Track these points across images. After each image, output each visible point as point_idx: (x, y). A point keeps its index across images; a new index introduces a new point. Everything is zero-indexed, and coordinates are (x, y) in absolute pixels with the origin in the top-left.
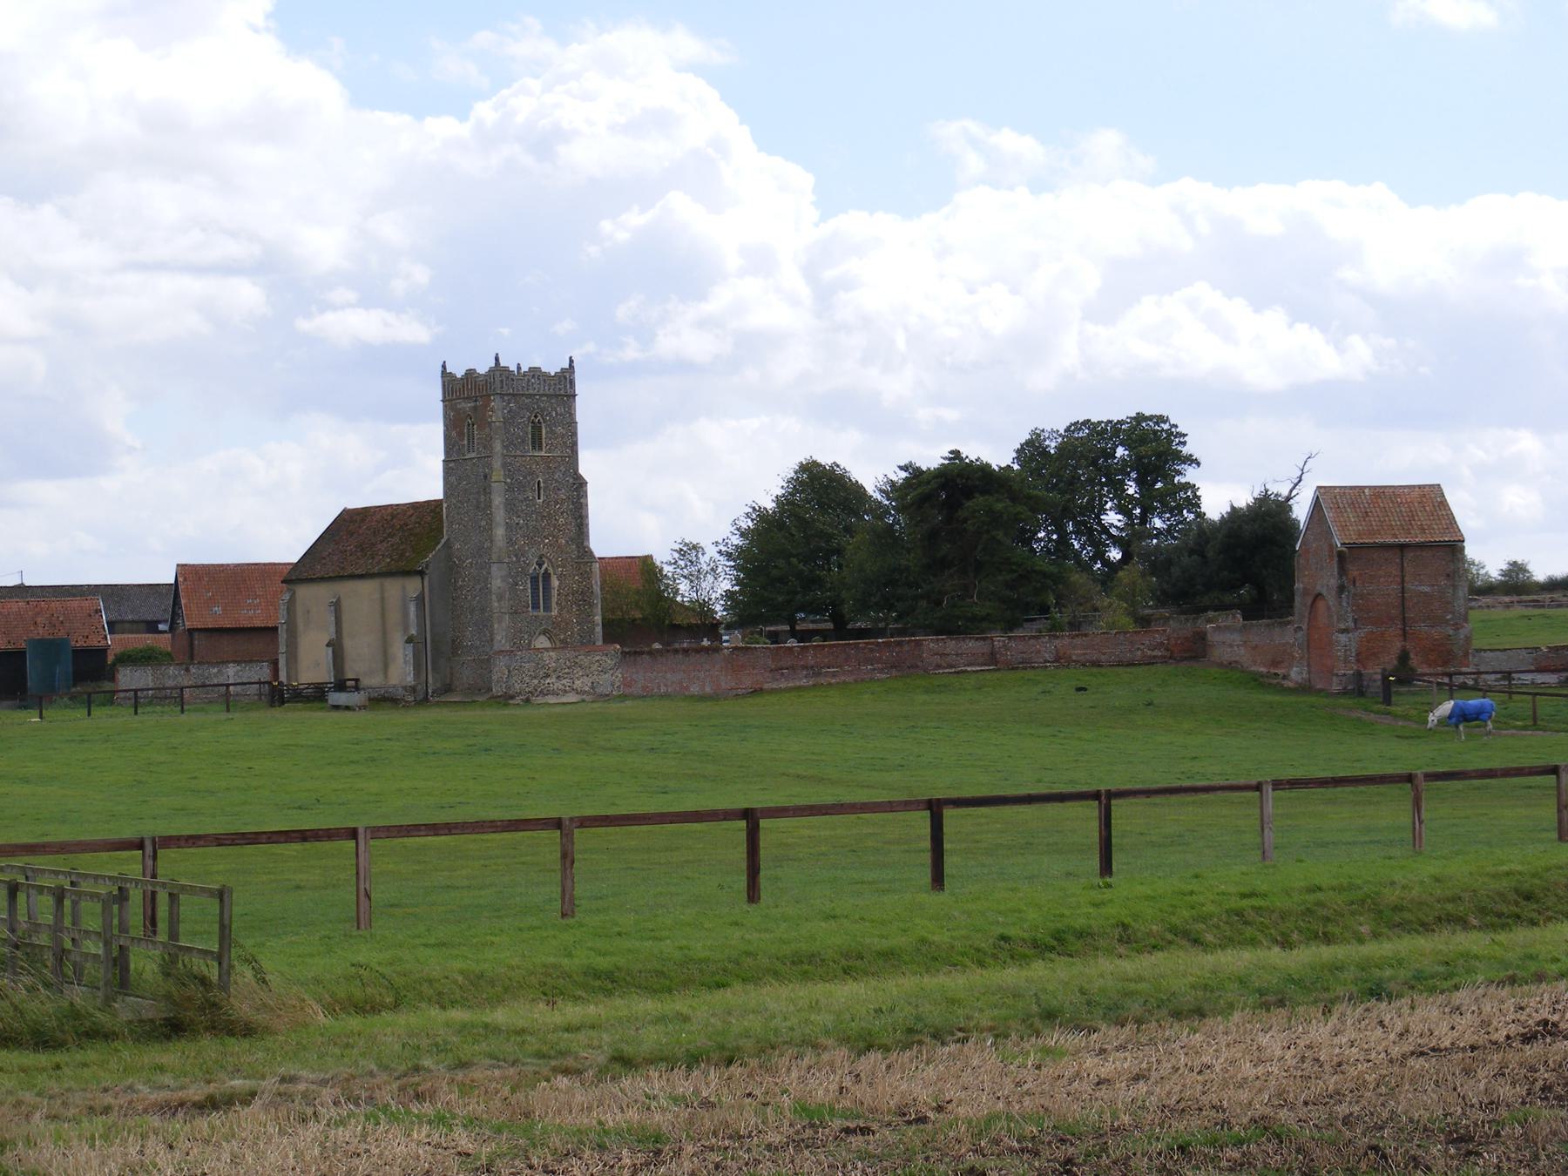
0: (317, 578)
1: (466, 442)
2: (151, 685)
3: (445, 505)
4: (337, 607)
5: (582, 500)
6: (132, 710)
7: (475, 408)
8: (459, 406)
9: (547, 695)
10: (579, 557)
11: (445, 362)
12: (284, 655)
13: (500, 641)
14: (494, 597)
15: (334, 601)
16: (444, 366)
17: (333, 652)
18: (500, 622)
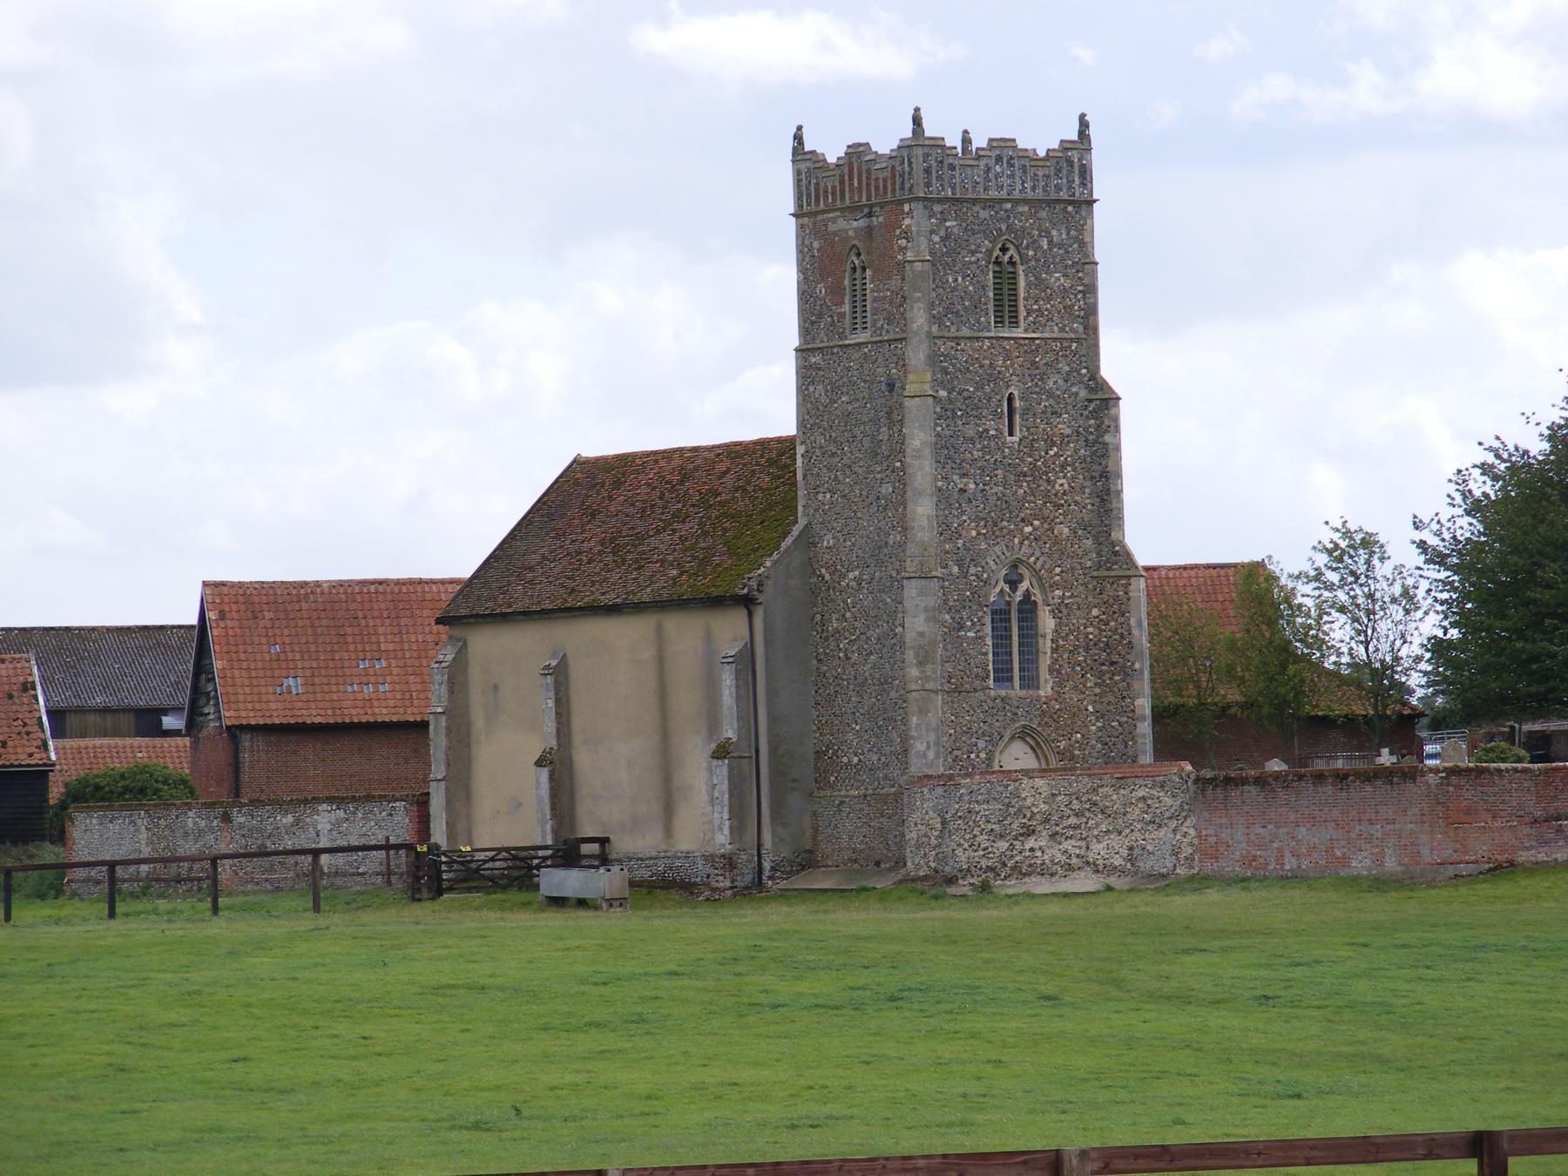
1: (847, 308)
2: (146, 852)
3: (800, 450)
4: (559, 675)
7: (869, 229)
8: (832, 227)
9: (1028, 874)
14: (910, 656)
15: (554, 663)
16: (798, 138)
17: (552, 778)
18: (923, 712)
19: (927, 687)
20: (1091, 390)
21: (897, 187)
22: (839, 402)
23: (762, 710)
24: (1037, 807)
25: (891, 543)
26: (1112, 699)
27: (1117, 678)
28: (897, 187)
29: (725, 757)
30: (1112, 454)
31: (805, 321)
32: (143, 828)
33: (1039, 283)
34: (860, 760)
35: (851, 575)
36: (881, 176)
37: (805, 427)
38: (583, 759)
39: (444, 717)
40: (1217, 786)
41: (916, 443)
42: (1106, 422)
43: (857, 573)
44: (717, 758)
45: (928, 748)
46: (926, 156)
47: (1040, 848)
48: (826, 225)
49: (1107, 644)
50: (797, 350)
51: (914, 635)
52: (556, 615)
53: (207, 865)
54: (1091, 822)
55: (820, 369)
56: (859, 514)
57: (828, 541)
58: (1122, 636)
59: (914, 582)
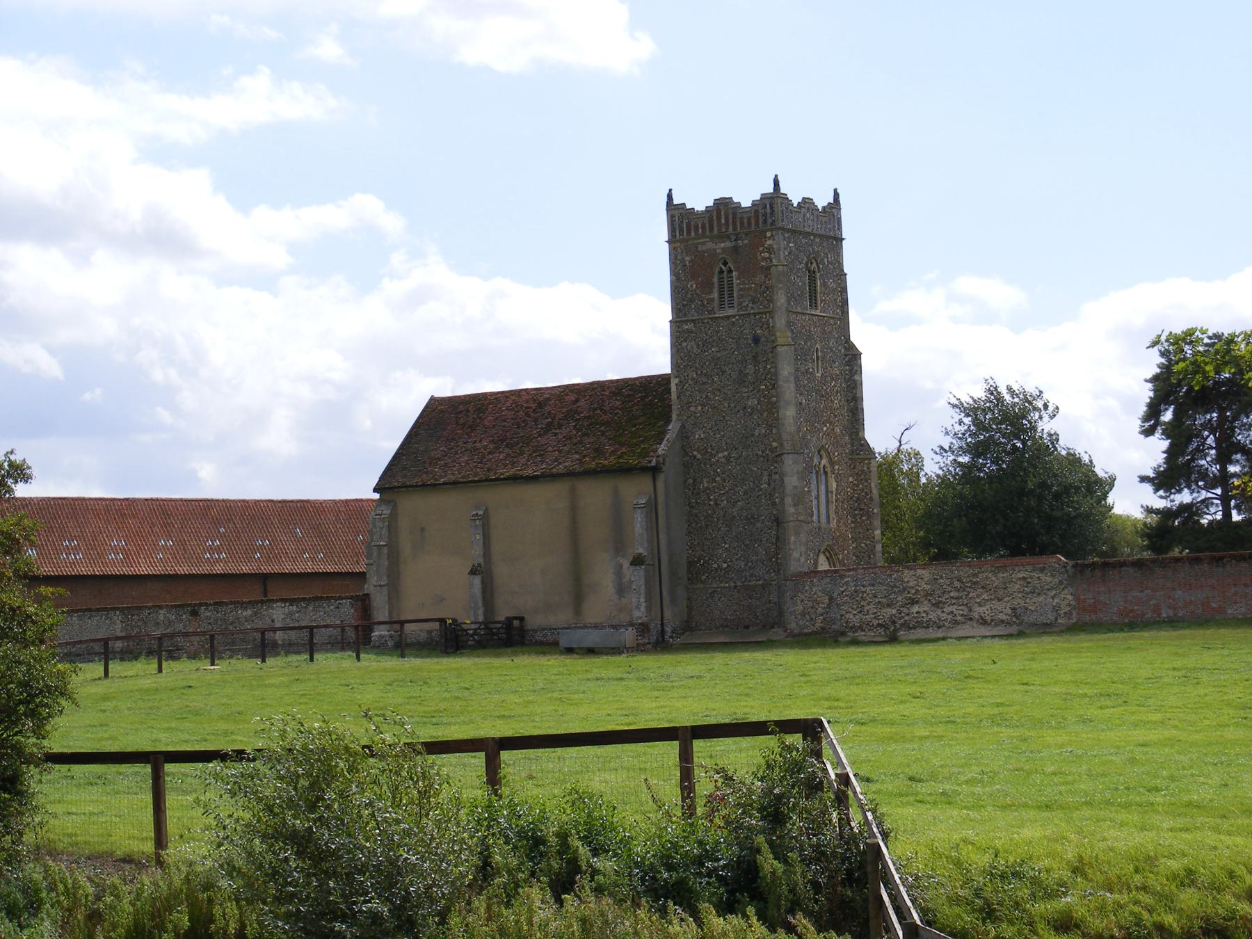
0: (444, 484)
1: (716, 295)
2: (119, 634)
3: (674, 382)
4: (484, 522)
5: (856, 377)
6: (307, 656)
7: (736, 249)
8: (700, 248)
9: (914, 628)
10: (852, 453)
11: (670, 190)
12: (386, 588)
13: (799, 560)
14: (788, 500)
15: (481, 512)
16: (670, 197)
17: (483, 582)
18: (797, 534)
19: (800, 518)
20: (846, 348)
21: (761, 221)
22: (710, 351)
23: (663, 537)
24: (920, 586)
25: (757, 434)
26: (861, 530)
27: (864, 518)
28: (761, 221)
29: (642, 564)
30: (859, 386)
31: (677, 304)
32: (118, 621)
33: (824, 284)
34: (728, 566)
35: (721, 455)
36: (745, 216)
37: (679, 367)
38: (501, 571)
39: (386, 548)
40: (1095, 568)
41: (785, 373)
42: (855, 368)
43: (726, 453)
44: (636, 565)
45: (801, 555)
46: (782, 203)
47: (925, 612)
48: (697, 247)
49: (858, 498)
50: (670, 321)
51: (791, 488)
52: (547, 479)
53: (306, 633)
54: (971, 595)
55: (692, 332)
56: (727, 418)
57: (700, 435)
58: (866, 493)
59: (791, 456)
